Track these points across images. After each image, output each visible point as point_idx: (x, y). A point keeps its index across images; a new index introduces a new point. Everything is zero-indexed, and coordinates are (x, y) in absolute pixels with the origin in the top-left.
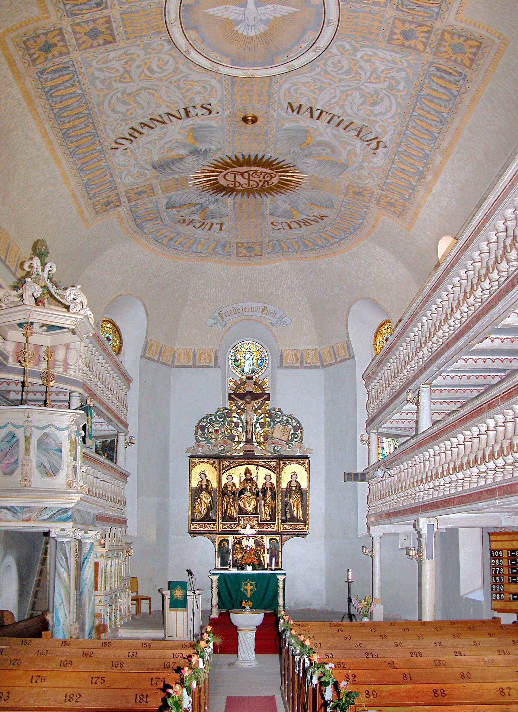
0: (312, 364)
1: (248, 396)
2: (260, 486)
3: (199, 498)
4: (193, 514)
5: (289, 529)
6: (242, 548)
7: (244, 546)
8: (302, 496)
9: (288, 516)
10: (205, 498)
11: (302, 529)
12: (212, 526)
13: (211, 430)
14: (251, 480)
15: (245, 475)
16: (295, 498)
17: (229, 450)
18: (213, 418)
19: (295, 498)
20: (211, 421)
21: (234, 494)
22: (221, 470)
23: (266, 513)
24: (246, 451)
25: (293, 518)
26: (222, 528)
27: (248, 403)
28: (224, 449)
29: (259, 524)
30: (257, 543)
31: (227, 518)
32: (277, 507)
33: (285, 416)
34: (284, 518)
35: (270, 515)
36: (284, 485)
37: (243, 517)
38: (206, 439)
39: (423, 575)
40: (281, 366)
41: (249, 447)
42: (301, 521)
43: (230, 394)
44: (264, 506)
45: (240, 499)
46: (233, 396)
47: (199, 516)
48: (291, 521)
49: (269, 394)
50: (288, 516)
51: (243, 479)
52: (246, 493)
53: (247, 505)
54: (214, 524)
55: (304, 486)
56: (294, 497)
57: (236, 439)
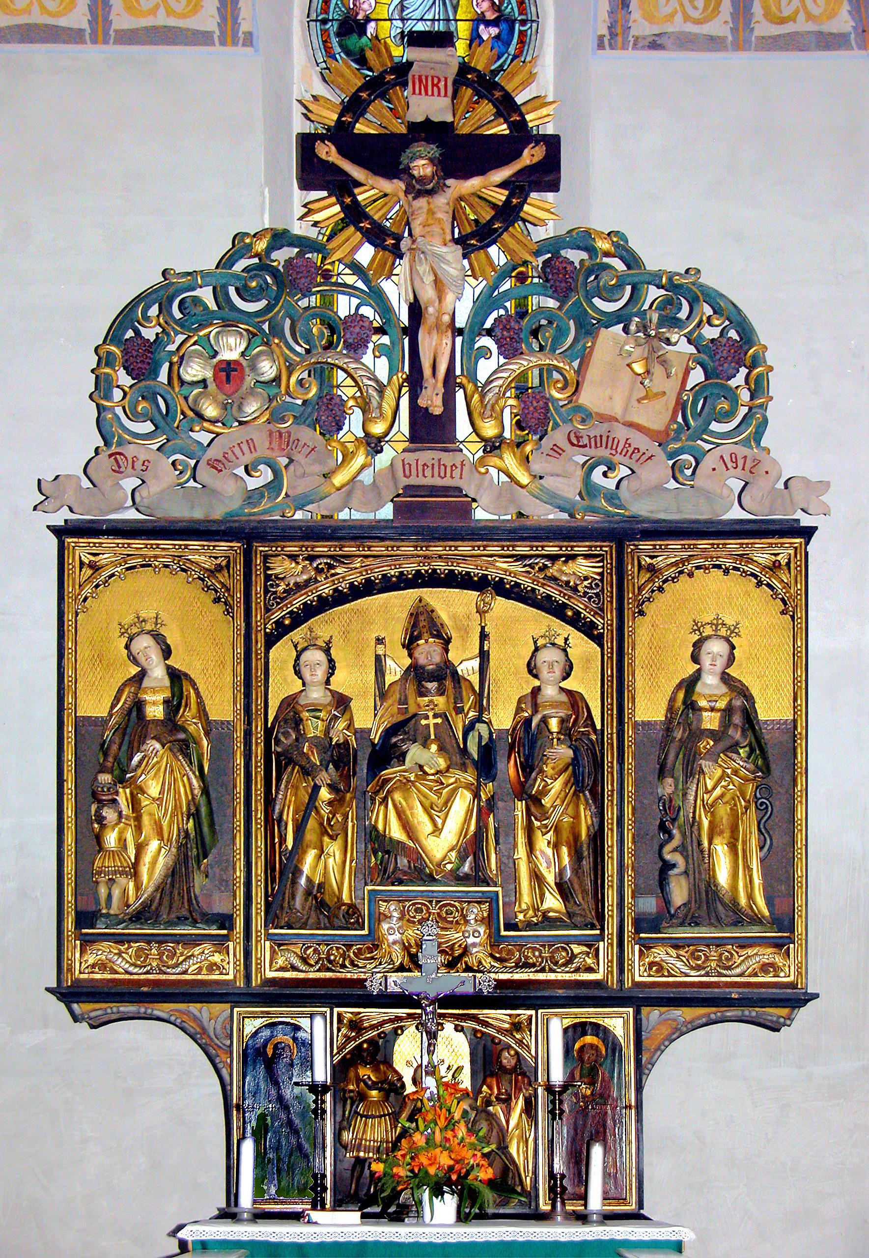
0: (802, 25)
1: (420, 148)
2: (502, 718)
3: (121, 780)
4: (86, 878)
5: (680, 969)
6: (392, 1088)
7: (407, 1075)
8: (766, 769)
9: (679, 892)
10: (162, 783)
11: (765, 968)
12: (205, 953)
13: (194, 371)
14: (446, 675)
15: (410, 645)
16: (720, 781)
17: (303, 487)
18: (206, 295)
19: (720, 781)
20: (194, 317)
21: (340, 756)
22: (266, 622)
23: (537, 877)
24: (410, 490)
25: (709, 904)
26: (272, 966)
27: (419, 189)
28: (275, 485)
29: (495, 940)
30: (487, 1058)
31: (285, 897)
32: (611, 840)
33: (655, 279)
34: (649, 904)
35: (563, 889)
36: (650, 707)
37: (401, 899)
38: (163, 422)
39: (642, 1188)
40: (615, 36)
41: (430, 468)
42: (756, 920)
43: (306, 142)
44: (530, 831)
45: (380, 791)
46: (327, 152)
47: (125, 894)
48: (695, 922)
49: (553, 144)
50: (679, 892)
51: (394, 671)
52: (415, 753)
53: (423, 824)
54: (220, 943)
55: (771, 708)
56: (712, 773)
57: (354, 424)
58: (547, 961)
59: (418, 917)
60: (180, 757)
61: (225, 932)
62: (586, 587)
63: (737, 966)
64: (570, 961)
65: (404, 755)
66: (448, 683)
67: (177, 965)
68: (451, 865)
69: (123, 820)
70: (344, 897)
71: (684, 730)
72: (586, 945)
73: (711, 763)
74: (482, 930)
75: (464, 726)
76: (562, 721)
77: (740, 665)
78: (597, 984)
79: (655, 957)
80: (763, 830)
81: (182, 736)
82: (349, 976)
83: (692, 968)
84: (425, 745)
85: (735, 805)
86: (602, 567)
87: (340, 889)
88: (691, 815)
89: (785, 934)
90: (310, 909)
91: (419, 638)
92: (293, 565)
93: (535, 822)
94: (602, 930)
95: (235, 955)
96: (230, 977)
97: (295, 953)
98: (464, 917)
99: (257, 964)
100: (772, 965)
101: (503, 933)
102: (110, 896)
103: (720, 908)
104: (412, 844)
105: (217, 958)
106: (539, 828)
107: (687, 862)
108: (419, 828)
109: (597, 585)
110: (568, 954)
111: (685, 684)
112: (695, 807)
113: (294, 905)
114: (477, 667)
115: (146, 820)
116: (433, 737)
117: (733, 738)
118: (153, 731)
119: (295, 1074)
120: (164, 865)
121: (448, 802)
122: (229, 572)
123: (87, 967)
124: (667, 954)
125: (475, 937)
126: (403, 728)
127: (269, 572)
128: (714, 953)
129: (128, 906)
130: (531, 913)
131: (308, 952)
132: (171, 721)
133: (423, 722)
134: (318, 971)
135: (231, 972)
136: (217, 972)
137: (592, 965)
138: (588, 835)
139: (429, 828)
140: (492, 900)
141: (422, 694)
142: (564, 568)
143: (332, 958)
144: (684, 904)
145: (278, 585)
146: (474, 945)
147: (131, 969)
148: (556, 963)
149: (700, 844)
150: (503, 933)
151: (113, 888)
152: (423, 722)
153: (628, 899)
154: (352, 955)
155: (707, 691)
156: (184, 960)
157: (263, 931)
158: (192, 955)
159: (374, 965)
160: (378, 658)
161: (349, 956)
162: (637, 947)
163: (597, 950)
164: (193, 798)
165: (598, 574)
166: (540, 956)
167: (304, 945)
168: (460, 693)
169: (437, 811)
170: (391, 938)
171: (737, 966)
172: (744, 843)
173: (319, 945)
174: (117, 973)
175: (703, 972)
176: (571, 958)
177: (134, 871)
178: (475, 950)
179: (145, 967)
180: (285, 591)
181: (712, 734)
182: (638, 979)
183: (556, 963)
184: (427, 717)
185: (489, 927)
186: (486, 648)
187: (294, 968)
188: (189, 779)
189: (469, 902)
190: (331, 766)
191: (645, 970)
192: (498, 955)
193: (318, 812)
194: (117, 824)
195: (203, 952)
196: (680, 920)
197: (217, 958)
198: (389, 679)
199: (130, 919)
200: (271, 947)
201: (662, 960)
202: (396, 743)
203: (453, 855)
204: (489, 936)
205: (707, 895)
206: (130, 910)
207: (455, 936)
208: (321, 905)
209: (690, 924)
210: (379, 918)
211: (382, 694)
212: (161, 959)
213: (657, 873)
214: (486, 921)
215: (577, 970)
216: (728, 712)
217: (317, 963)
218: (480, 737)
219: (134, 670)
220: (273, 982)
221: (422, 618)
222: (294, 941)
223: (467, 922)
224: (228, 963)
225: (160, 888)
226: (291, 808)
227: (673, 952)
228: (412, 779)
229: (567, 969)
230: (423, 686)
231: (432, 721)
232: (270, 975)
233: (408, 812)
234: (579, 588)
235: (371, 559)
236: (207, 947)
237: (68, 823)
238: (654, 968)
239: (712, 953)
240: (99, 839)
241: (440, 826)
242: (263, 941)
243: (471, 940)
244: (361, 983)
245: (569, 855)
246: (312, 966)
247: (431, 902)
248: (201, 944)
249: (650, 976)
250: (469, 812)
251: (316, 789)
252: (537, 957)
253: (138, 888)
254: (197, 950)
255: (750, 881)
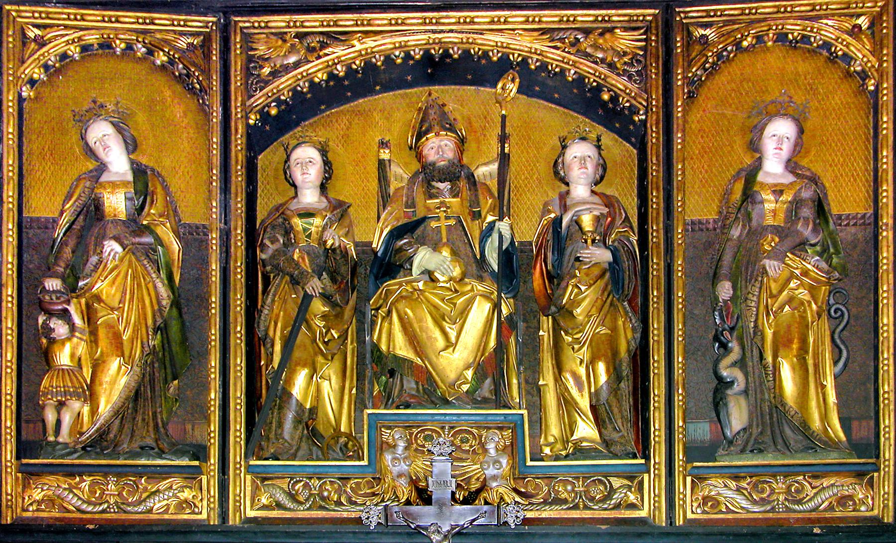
9: (738, 416)
25: (776, 424)
29: (519, 473)
34: (703, 430)
42: (831, 445)
50: (738, 416)
52: (423, 258)
54: (192, 475)
60: (145, 262)
61: (196, 463)
62: (625, 63)
63: (810, 500)
64: (608, 497)
65: (410, 260)
66: (462, 183)
67: (140, 502)
68: (468, 385)
69: (77, 334)
71: (744, 226)
72: (627, 478)
73: (776, 263)
74: (504, 461)
75: (482, 232)
76: (597, 220)
78: (642, 521)
80: (838, 341)
81: (148, 239)
82: (345, 515)
83: (755, 502)
84: (436, 247)
85: (805, 311)
86: (645, 40)
87: (338, 421)
88: (752, 325)
89: (870, 461)
90: (301, 439)
91: (427, 132)
92: (280, 42)
93: (565, 337)
94: (647, 457)
95: (209, 491)
96: (204, 516)
98: (482, 445)
99: (235, 501)
100: (850, 497)
101: (529, 463)
102: (59, 423)
103: (788, 431)
104: (419, 362)
105: (187, 494)
106: (569, 344)
107: (747, 380)
108: (429, 344)
109: (638, 62)
110: (606, 488)
111: (744, 173)
112: (757, 315)
113: (281, 434)
115: (102, 333)
116: (445, 240)
117: (802, 233)
118: (112, 231)
120: (125, 386)
121: (464, 312)
123: (31, 504)
124: (726, 486)
125: (495, 467)
126: (410, 229)
128: (779, 485)
129: (82, 434)
130: (559, 446)
131: (297, 488)
132: (135, 225)
133: (434, 224)
134: (308, 509)
135: (205, 512)
136: (188, 511)
138: (628, 351)
139: (441, 343)
140: (516, 426)
141: (431, 196)
142: (601, 41)
143: (326, 494)
144: (744, 429)
145: (262, 67)
146: (495, 478)
147: (84, 506)
149: (761, 357)
150: (529, 463)
151: (62, 412)
152: (434, 224)
153: (679, 422)
154: (349, 490)
155: (770, 181)
156: (148, 497)
157: (243, 463)
158: (158, 491)
161: (345, 491)
162: (689, 479)
163: (641, 483)
164: (160, 310)
165: (640, 48)
166: (573, 490)
167: (292, 479)
168: (476, 196)
169: (451, 317)
170: (396, 470)
171: (810, 500)
172: (816, 356)
173: (311, 478)
174: (69, 511)
175: (769, 508)
176: (609, 493)
177: (90, 394)
178: (494, 484)
179: (101, 504)
180: (271, 74)
181: (776, 230)
182: (690, 516)
183: (592, 499)
185: (512, 456)
186: (506, 150)
187: (279, 506)
188: (155, 287)
189: (489, 428)
190: (325, 275)
192: (523, 490)
193: (309, 327)
194: (69, 339)
195: (171, 487)
196: (739, 448)
197: (187, 494)
198: (393, 186)
199: (83, 448)
200: (253, 482)
201: (719, 494)
202: (402, 246)
203: (469, 374)
204: (513, 467)
205: (771, 418)
206: (84, 438)
207: (472, 468)
208: (314, 434)
209: (752, 451)
210: (380, 447)
211: (385, 199)
213: (711, 394)
215: (617, 506)
216: (796, 204)
217: (307, 500)
218: (501, 237)
219: (91, 165)
220: (254, 520)
221: (431, 112)
223: (486, 451)
224: (201, 500)
225: (119, 413)
226: (279, 325)
227: (733, 484)
228: (421, 288)
229: (606, 506)
230: (433, 187)
231: (443, 224)
232: (251, 514)
233: (416, 326)
236: (177, 482)
237: (7, 334)
238: (710, 504)
239: (780, 485)
240: (47, 356)
241: (453, 340)
242: (242, 475)
243: (491, 471)
244: (358, 521)
245: (608, 371)
247: (443, 428)
248: (167, 478)
249: (704, 512)
250: (489, 322)
251: (307, 299)
252: (569, 492)
253: (94, 412)
254: (163, 485)
255: (824, 400)
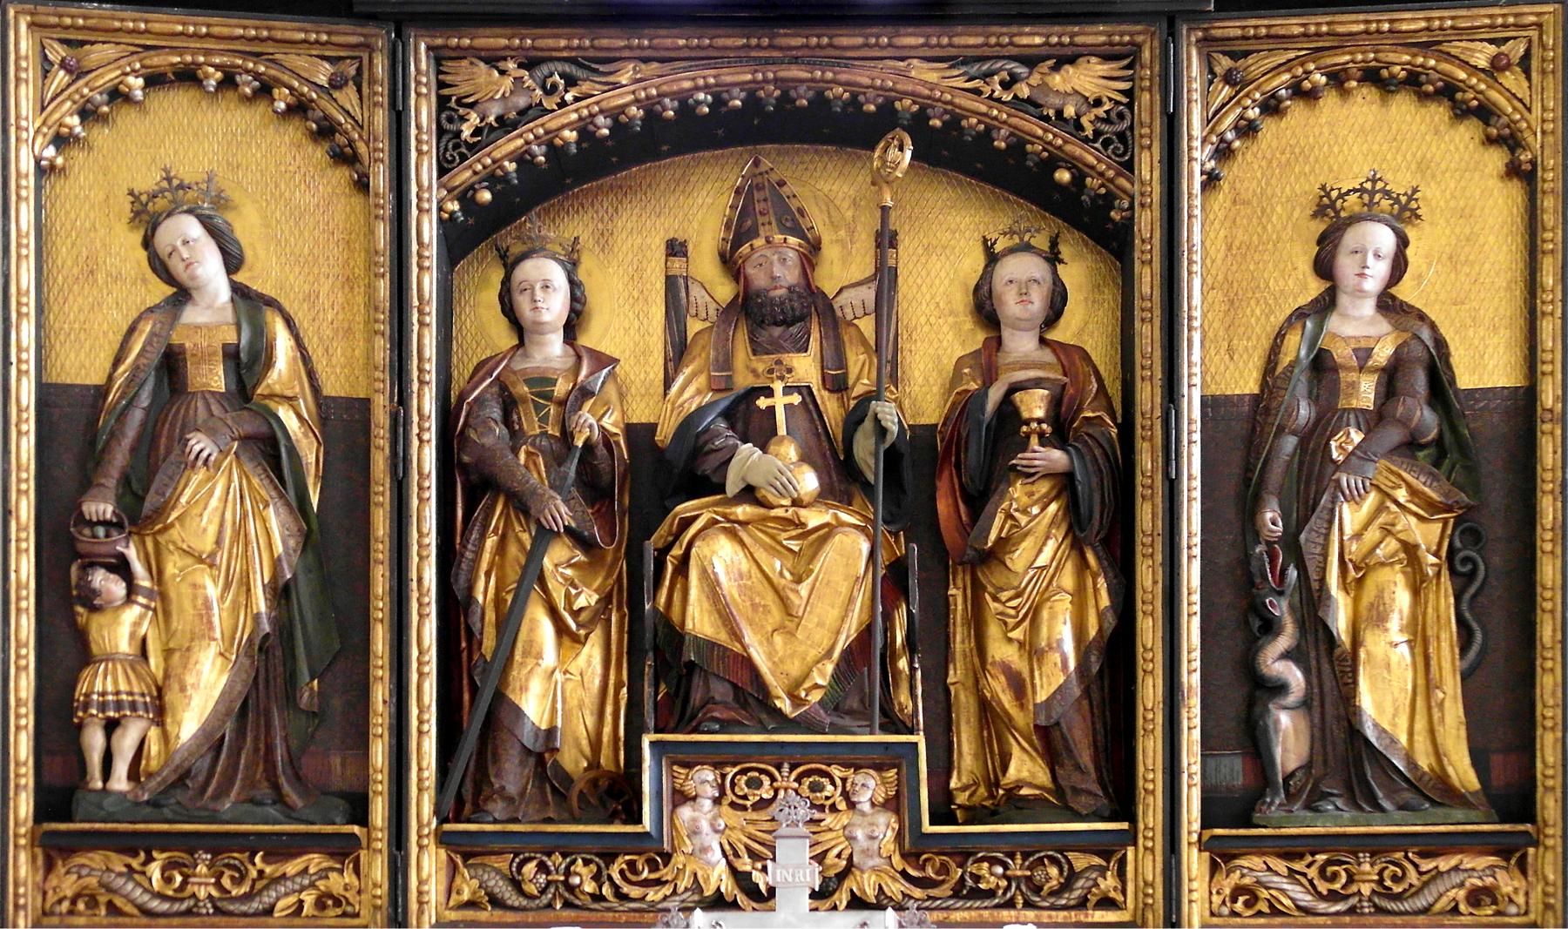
54: (344, 850)
58: (1018, 887)
59: (753, 799)
64: (1066, 886)
70: (602, 761)
72: (1099, 854)
77: (1419, 277)
79: (1243, 876)
97: (498, 871)
101: (927, 828)
105: (336, 883)
114: (871, 305)
119: (1277, 802)
122: (359, 91)
127: (446, 92)
130: (982, 791)
133: (762, 403)
137: (1112, 894)
145: (463, 119)
148: (1037, 890)
154: (616, 877)
159: (660, 895)
160: (671, 282)
161: (610, 878)
163: (1122, 863)
167: (516, 855)
173: (549, 855)
179: (182, 900)
180: (477, 131)
183: (1037, 890)
184: (769, 392)
186: (891, 263)
191: (1224, 902)
211: (678, 351)
212: (218, 885)
214: (894, 803)
215: (1082, 904)
217: (543, 892)
222: (496, 847)
227: (1280, 865)
234: (1084, 121)
235: (655, 65)
238: (1241, 899)
246: (531, 897)
247: (779, 768)
254: (292, 868)
